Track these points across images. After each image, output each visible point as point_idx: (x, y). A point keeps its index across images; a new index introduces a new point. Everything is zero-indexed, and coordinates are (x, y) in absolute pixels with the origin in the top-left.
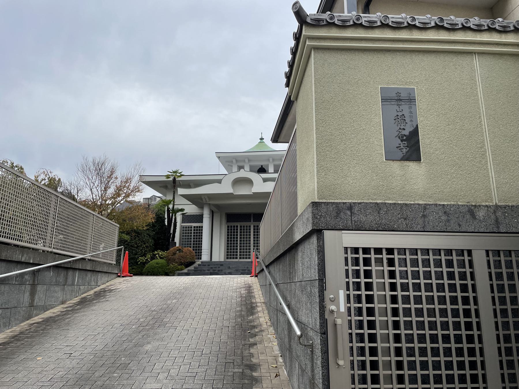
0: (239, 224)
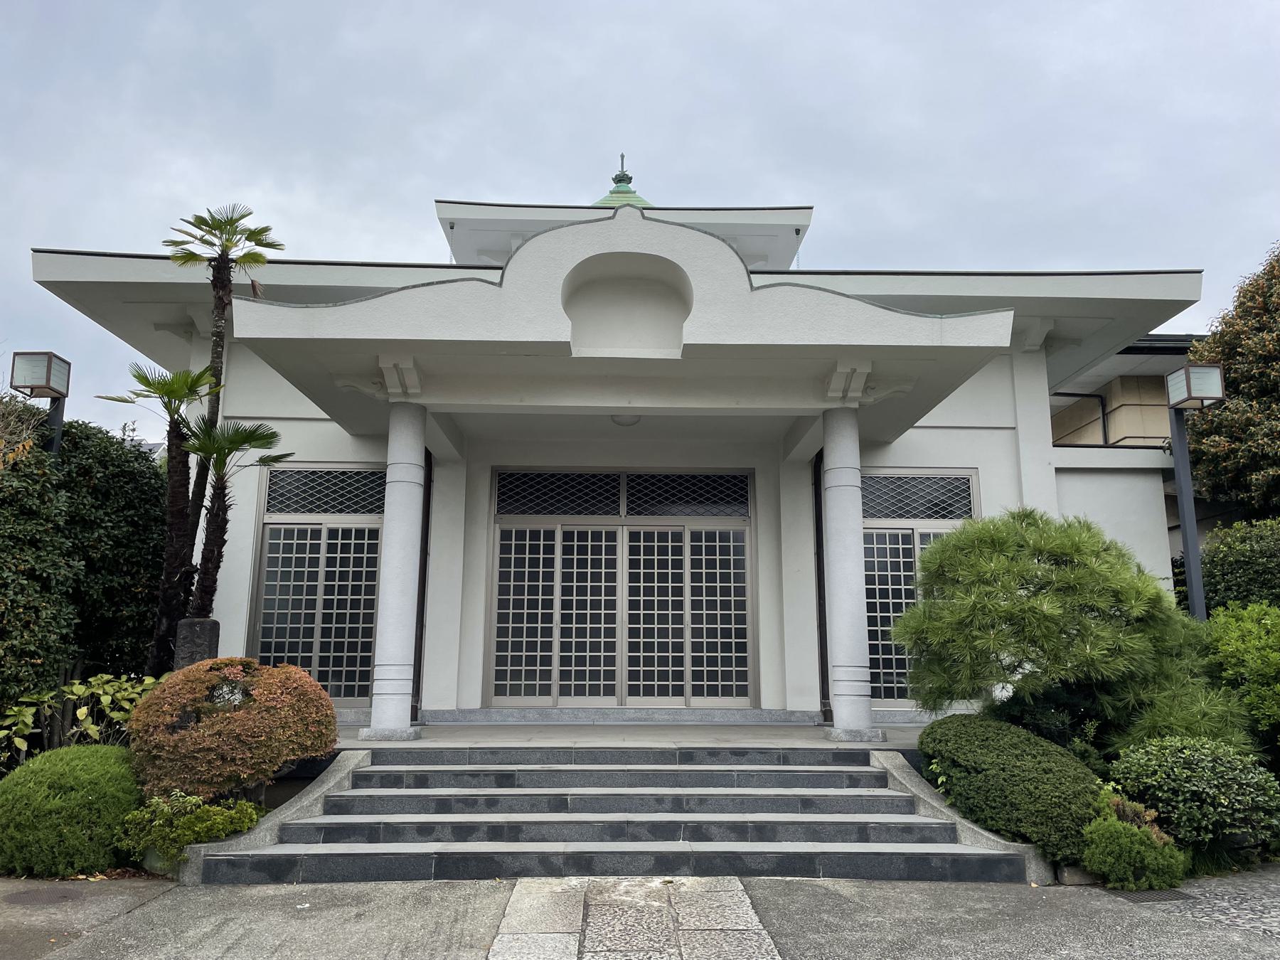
0: (558, 524)
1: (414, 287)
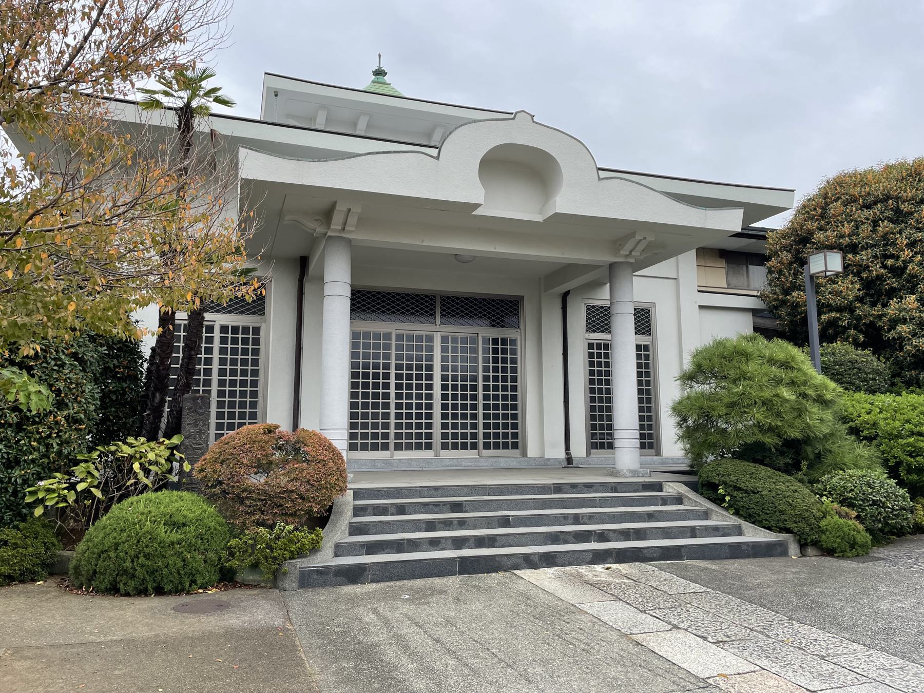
1: (377, 153)
